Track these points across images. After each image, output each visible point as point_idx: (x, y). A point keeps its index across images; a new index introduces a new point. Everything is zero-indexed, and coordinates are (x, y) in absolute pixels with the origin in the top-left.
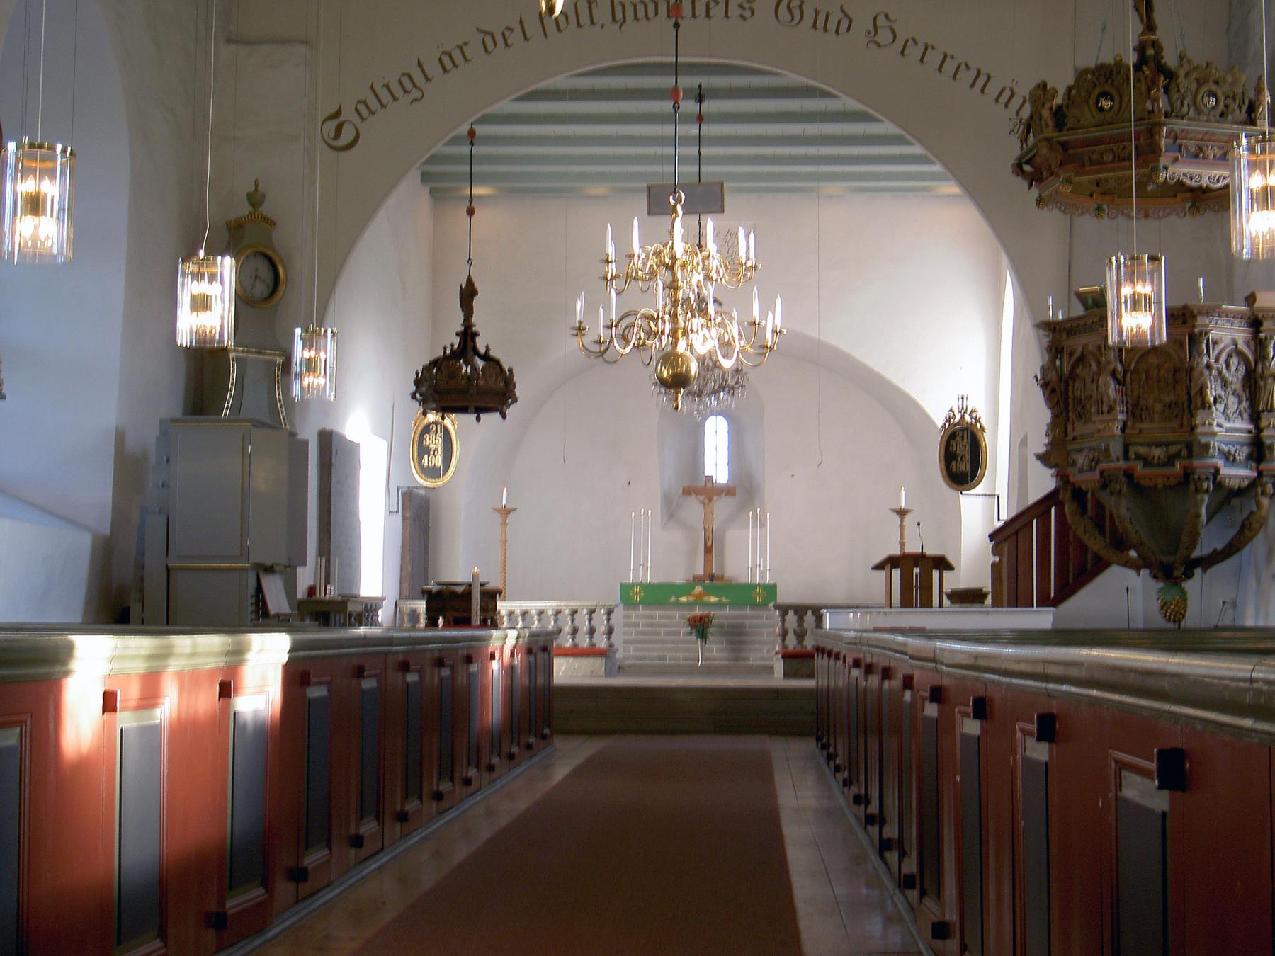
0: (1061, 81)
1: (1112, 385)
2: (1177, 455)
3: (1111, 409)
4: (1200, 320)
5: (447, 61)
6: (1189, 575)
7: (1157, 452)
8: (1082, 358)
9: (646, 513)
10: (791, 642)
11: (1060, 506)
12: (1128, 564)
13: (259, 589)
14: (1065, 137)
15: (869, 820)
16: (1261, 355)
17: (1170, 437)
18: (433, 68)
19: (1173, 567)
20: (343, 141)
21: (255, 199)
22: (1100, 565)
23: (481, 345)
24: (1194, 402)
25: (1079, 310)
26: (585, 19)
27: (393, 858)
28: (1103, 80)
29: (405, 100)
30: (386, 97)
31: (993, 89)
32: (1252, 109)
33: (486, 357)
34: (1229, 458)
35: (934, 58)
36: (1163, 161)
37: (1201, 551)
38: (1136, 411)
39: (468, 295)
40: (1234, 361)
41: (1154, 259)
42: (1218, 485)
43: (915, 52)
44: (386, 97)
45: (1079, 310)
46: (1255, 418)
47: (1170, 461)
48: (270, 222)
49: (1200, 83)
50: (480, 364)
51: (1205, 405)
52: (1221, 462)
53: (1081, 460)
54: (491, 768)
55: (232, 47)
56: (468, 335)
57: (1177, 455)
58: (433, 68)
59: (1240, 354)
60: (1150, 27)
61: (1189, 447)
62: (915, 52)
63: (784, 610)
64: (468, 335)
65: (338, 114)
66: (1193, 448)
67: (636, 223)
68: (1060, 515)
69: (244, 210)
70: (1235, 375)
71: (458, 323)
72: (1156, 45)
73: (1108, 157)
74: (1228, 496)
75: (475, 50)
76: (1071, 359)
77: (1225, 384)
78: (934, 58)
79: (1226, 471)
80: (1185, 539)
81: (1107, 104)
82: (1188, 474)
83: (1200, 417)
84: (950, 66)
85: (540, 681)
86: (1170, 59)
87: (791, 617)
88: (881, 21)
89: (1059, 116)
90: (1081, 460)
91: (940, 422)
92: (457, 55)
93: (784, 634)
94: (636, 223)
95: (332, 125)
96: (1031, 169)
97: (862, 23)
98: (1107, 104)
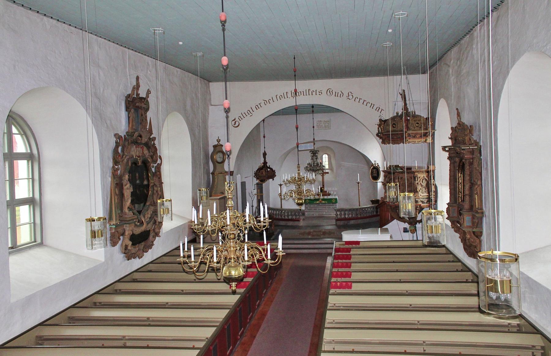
4: (416, 173)
5: (257, 107)
18: (254, 109)
23: (268, 165)
26: (286, 97)
27: (478, 89)
30: (244, 115)
31: (375, 108)
33: (269, 168)
34: (423, 202)
35: (362, 101)
39: (265, 154)
40: (424, 181)
43: (357, 100)
44: (244, 115)
46: (429, 193)
48: (222, 146)
52: (420, 203)
54: (470, 126)
56: (265, 163)
58: (254, 109)
62: (357, 100)
64: (265, 163)
65: (235, 120)
69: (216, 143)
70: (424, 184)
71: (262, 160)
75: (262, 104)
77: (422, 186)
78: (362, 101)
84: (365, 103)
85: (31, 196)
88: (350, 94)
92: (259, 106)
95: (234, 122)
97: (346, 94)
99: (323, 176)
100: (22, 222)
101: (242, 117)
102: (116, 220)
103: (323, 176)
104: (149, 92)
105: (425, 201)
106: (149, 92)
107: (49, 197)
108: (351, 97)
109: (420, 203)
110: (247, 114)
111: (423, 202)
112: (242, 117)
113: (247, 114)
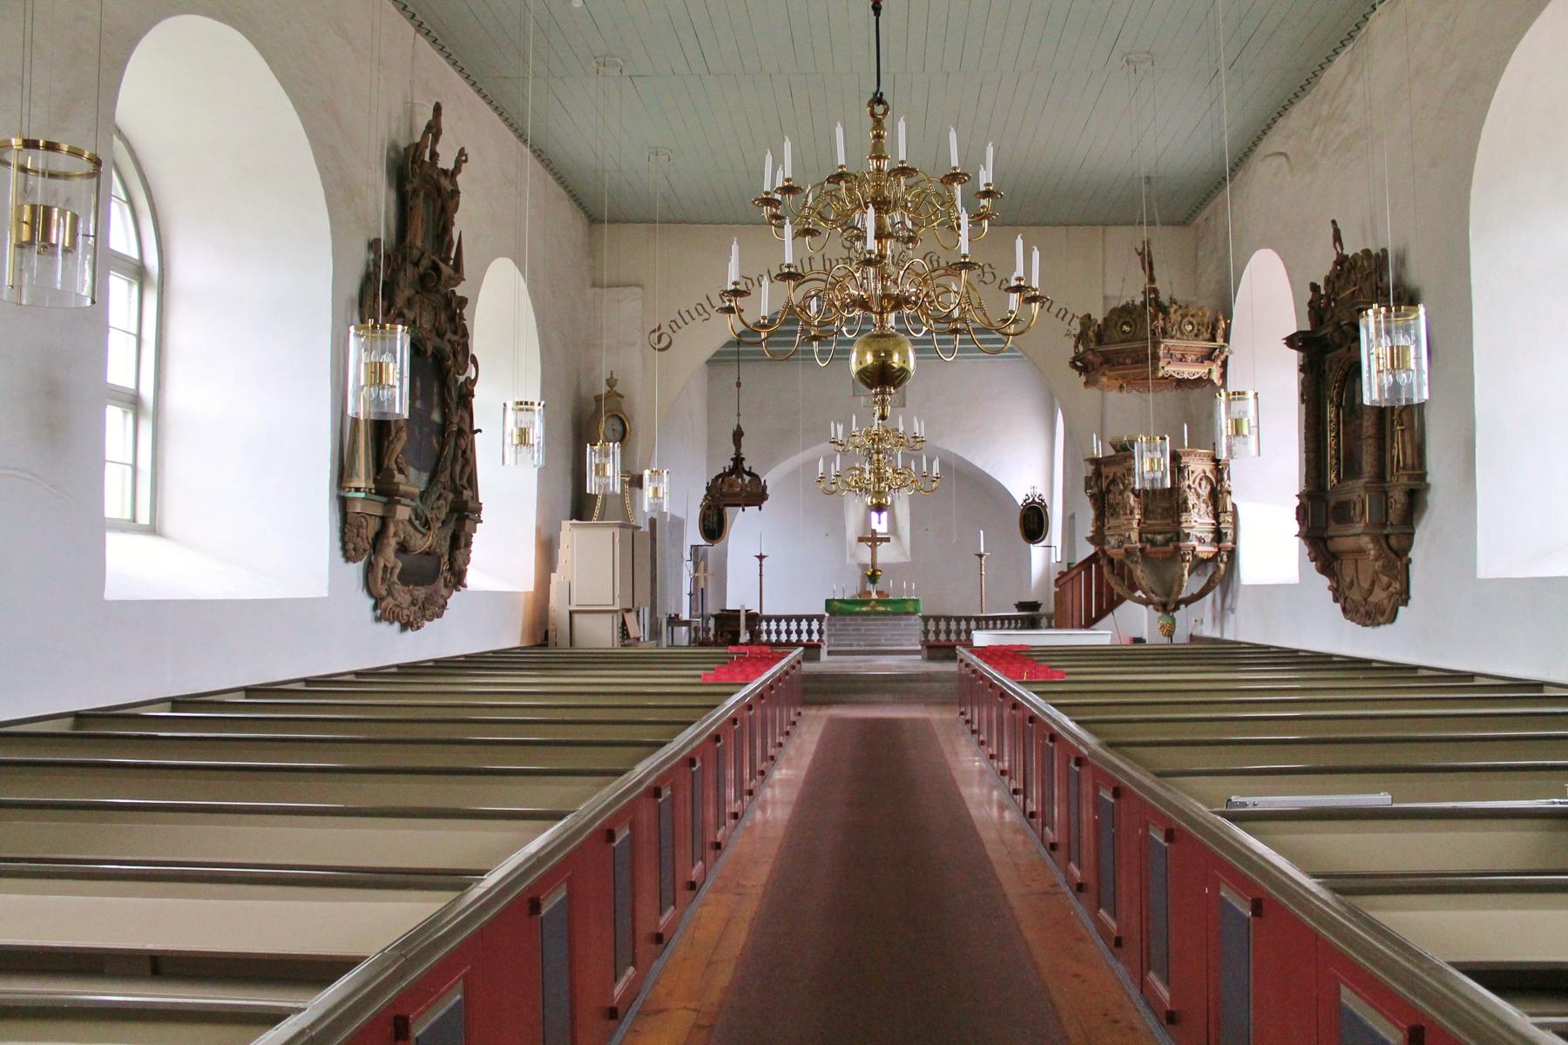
0: (1099, 316)
1: (1132, 497)
2: (1171, 540)
3: (1132, 512)
4: (1184, 460)
6: (1176, 608)
7: (1159, 538)
8: (1113, 481)
9: (989, 715)
10: (932, 637)
11: (1097, 563)
12: (1139, 601)
13: (624, 623)
14: (1102, 349)
15: (973, 732)
16: (1220, 480)
17: (1167, 528)
19: (1168, 604)
20: (662, 345)
21: (611, 382)
22: (1121, 600)
23: (746, 466)
24: (1183, 507)
25: (1111, 452)
28: (1125, 314)
29: (699, 319)
30: (687, 318)
31: (1054, 309)
32: (1214, 328)
33: (750, 473)
34: (1200, 540)
36: (1161, 364)
37: (1184, 594)
38: (1146, 513)
39: (738, 435)
41: (1163, 439)
42: (1194, 556)
44: (687, 318)
45: (1111, 452)
46: (1216, 516)
47: (1166, 543)
49: (1183, 316)
50: (747, 478)
51: (1186, 510)
52: (1195, 543)
53: (1113, 541)
55: (597, 290)
56: (738, 460)
57: (1171, 540)
59: (1207, 478)
60: (1152, 279)
61: (1178, 534)
63: (926, 619)
64: (738, 460)
66: (1178, 535)
67: (735, 248)
68: (1099, 569)
70: (1205, 491)
72: (1155, 291)
73: (1128, 361)
74: (1199, 564)
76: (1103, 481)
79: (1199, 548)
80: (1175, 589)
81: (1126, 328)
82: (1178, 549)
83: (1184, 517)
86: (1164, 298)
87: (931, 625)
89: (1099, 339)
90: (1113, 541)
91: (1020, 502)
93: (926, 632)
94: (735, 248)
96: (1085, 366)
98: (1126, 328)
99: (873, 548)
100: (132, 386)
101: (680, 323)
102: (367, 477)
103: (873, 548)
104: (461, 158)
105: (1209, 537)
106: (461, 158)
107: (179, 396)
108: (989, 278)
109: (1195, 543)
110: (695, 314)
111: (1200, 540)
112: (680, 323)
113: (695, 314)
